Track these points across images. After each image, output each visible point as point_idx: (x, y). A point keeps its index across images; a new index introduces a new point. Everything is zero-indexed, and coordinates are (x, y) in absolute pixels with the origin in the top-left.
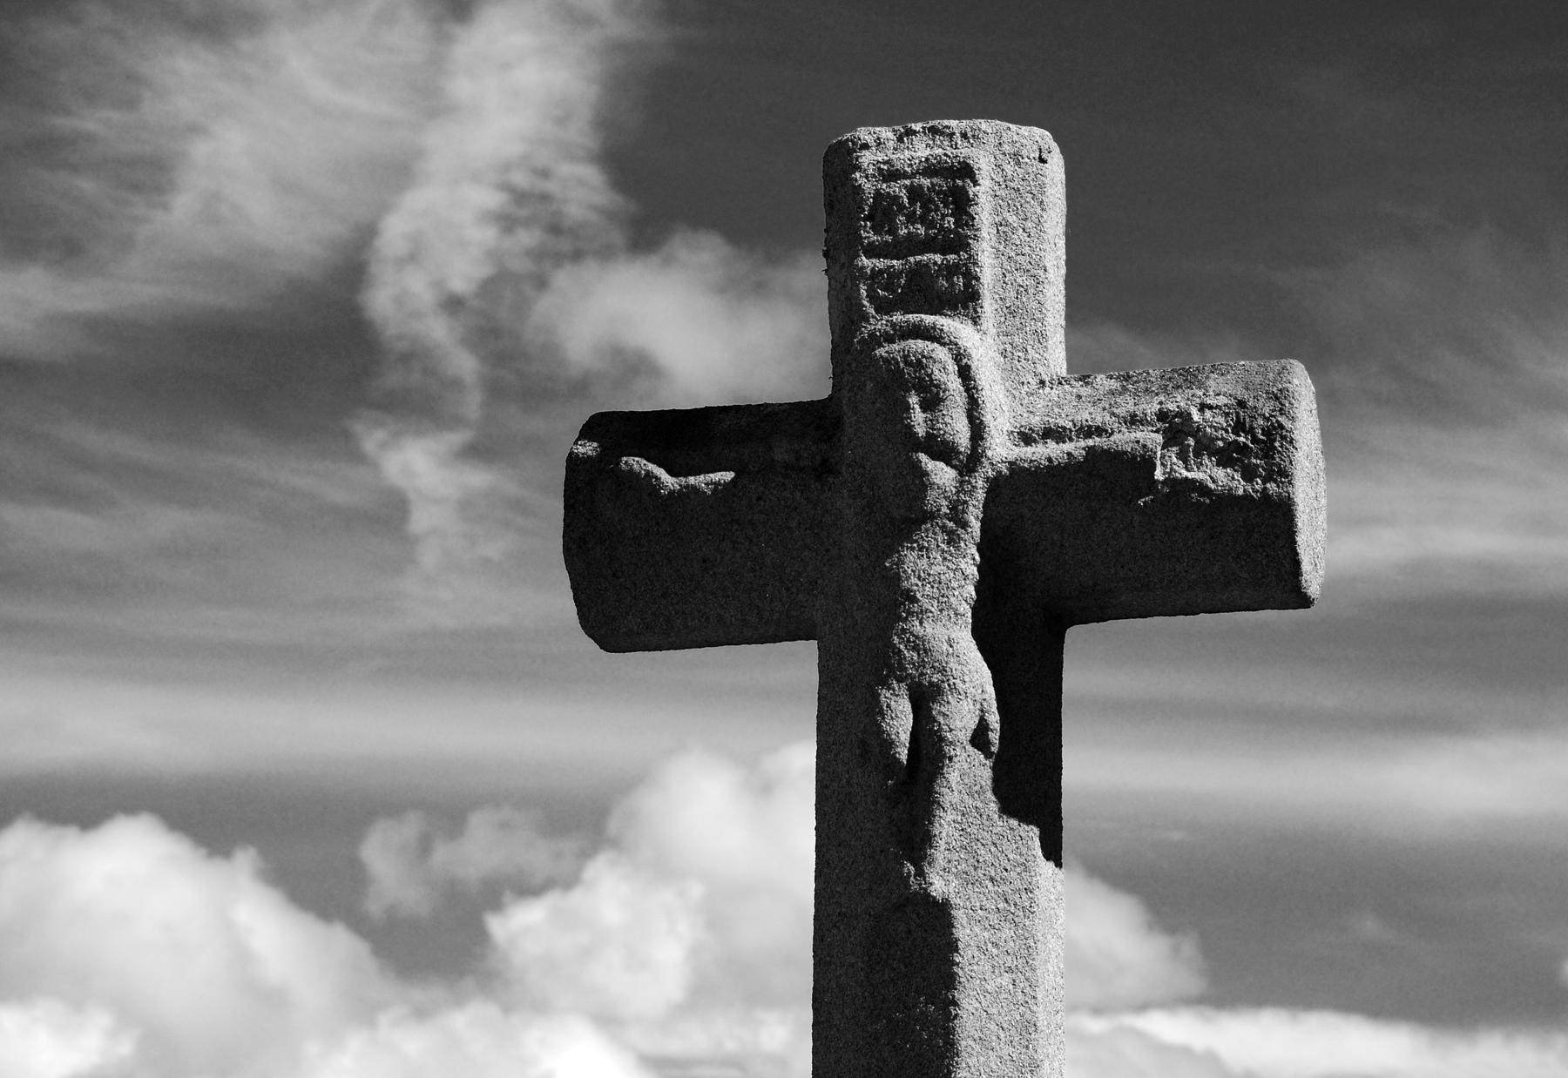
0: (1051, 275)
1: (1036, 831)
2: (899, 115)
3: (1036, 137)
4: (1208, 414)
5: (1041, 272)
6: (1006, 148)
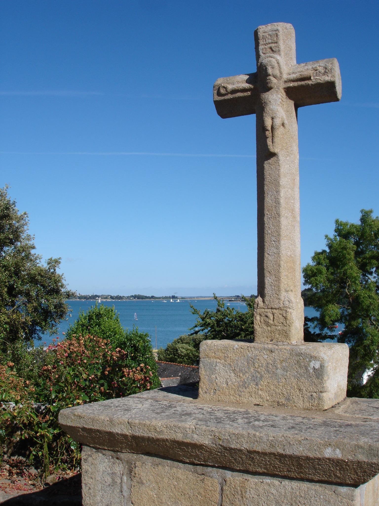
0: (293, 48)
1: (265, 162)
2: (265, 23)
3: (289, 26)
4: (320, 67)
5: (291, 48)
6: (284, 27)
